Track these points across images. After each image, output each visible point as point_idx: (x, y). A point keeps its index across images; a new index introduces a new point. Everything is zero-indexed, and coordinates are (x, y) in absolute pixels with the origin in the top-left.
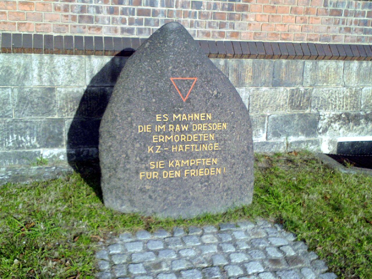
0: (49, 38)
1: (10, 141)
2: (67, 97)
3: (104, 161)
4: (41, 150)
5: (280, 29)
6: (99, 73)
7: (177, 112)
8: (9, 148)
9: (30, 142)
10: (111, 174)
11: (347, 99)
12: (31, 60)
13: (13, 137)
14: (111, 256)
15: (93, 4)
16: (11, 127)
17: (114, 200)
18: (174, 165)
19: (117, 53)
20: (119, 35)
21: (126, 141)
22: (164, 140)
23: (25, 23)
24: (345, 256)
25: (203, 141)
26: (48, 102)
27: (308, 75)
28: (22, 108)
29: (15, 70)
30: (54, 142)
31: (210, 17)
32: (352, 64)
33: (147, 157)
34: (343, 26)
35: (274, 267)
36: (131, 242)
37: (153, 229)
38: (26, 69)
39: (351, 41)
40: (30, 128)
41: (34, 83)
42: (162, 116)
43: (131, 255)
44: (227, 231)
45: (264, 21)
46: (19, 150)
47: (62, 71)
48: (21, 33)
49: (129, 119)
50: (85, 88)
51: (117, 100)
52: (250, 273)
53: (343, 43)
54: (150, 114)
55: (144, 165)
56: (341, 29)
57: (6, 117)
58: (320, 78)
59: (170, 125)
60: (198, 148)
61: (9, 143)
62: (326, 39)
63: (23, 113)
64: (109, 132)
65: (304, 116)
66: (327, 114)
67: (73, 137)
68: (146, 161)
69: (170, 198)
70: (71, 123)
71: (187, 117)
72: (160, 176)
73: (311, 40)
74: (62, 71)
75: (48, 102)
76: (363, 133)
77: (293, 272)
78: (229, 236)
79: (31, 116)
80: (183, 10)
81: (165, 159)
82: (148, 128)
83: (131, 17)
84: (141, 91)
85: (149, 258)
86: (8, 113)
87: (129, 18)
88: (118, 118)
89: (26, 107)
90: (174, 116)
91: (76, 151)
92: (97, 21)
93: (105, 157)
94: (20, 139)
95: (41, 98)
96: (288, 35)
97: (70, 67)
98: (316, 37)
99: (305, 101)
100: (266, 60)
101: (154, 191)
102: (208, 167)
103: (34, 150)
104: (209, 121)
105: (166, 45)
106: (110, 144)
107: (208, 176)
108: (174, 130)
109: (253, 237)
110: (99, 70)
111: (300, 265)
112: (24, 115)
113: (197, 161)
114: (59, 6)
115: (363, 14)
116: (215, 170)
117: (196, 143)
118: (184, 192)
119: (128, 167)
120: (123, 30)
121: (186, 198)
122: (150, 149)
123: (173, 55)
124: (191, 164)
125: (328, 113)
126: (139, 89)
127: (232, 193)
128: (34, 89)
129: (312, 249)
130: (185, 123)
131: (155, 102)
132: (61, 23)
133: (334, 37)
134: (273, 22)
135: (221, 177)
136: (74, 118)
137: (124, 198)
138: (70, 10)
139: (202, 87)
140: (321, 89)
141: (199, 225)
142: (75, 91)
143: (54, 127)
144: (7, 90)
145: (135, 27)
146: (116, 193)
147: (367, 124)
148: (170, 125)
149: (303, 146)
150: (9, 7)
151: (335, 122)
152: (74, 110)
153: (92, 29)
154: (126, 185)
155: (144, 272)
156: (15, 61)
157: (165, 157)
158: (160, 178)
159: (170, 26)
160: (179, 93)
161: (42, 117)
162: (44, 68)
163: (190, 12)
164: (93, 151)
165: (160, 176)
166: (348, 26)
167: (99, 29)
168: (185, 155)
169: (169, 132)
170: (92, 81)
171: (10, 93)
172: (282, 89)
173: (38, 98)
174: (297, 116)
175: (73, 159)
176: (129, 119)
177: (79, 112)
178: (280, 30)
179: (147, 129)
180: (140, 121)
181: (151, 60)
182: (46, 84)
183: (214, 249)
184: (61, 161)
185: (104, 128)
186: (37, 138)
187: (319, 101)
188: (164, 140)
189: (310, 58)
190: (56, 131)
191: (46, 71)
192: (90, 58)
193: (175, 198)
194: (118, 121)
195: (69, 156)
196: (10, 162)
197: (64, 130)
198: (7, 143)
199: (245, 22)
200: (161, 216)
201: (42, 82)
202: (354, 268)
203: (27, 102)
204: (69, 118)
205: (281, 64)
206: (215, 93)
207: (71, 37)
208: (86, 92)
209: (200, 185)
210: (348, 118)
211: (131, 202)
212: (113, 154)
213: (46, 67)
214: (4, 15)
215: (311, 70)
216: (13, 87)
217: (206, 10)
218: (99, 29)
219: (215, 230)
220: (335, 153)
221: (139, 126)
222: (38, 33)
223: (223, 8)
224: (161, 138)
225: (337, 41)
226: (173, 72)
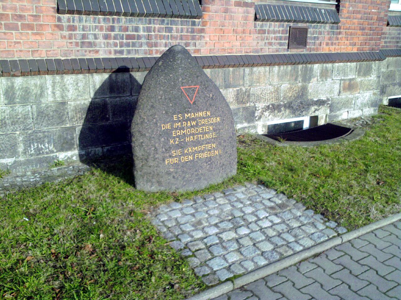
0: (58, 61)
1: (32, 149)
2: (76, 109)
3: (137, 154)
4: (57, 154)
5: (227, 46)
6: (100, 87)
7: (188, 112)
8: (31, 155)
9: (48, 148)
10: (144, 163)
11: (272, 94)
12: (46, 80)
13: (34, 145)
14: (163, 222)
15: (92, 32)
16: (32, 137)
17: (145, 183)
18: (188, 151)
19: (114, 70)
20: (113, 56)
21: (154, 137)
22: (181, 133)
23: (37, 51)
24: (313, 199)
25: (205, 132)
26: (61, 114)
27: (247, 78)
28: (40, 121)
29: (33, 90)
30: (67, 146)
31: (179, 39)
32: (274, 69)
33: (170, 147)
34: (267, 41)
35: (274, 212)
36: (170, 211)
37: (181, 200)
38: (42, 88)
39: (273, 52)
40: (48, 137)
41: (49, 99)
42: (178, 116)
43: (176, 219)
44: (230, 194)
45: (216, 40)
46: (40, 156)
47: (71, 88)
48: (35, 58)
49: (155, 120)
50: (90, 100)
51: (143, 107)
52: (261, 218)
53: (268, 54)
54: (169, 115)
55: (168, 154)
56: (265, 43)
57: (27, 129)
58: (255, 80)
59: (184, 122)
60: (203, 137)
61: (31, 151)
62: (257, 51)
63: (42, 125)
64: (140, 131)
65: (246, 109)
66: (260, 106)
67: (83, 141)
68: (170, 151)
69: (187, 176)
70: (80, 129)
71: (195, 115)
72: (180, 161)
73: (247, 52)
74: (71, 88)
75: (61, 114)
76: (283, 118)
77: (286, 213)
78: (233, 197)
79: (48, 126)
80: (159, 34)
81: (182, 148)
82: (168, 126)
83: (121, 41)
84: (161, 98)
85: (191, 219)
86: (29, 126)
87: (120, 42)
88: (146, 121)
89: (44, 119)
90: (186, 115)
91: (85, 152)
92: (95, 46)
93: (138, 151)
94: (40, 147)
95: (56, 111)
96: (232, 49)
97: (77, 84)
98: (250, 50)
99: (246, 97)
100: (220, 69)
101: (176, 173)
102: (210, 150)
103: (52, 155)
104: (209, 117)
105: (175, 63)
106: (141, 140)
107: (210, 157)
108: (187, 125)
109: (249, 195)
110: (100, 85)
111: (288, 208)
112: (42, 126)
113: (203, 147)
114: (64, 34)
115: (279, 32)
116: (214, 152)
117: (201, 133)
118: (196, 171)
119: (157, 156)
120: (116, 52)
121: (197, 175)
122: (172, 142)
123: (182, 70)
124: (199, 149)
125: (261, 105)
126: (160, 97)
127: (225, 168)
128: (49, 104)
129: (290, 197)
130: (194, 119)
131: (172, 106)
132: (66, 49)
133: (261, 49)
134: (222, 40)
135: (218, 157)
136: (83, 125)
137: (154, 180)
138: (73, 38)
139: (202, 92)
140: (256, 88)
141: (209, 193)
142: (82, 103)
143: (67, 134)
144: (27, 107)
145: (124, 48)
146: (147, 178)
147: (285, 110)
148: (184, 122)
149: (247, 131)
150: (23, 38)
151: (265, 111)
152: (82, 118)
153: (92, 52)
154: (155, 171)
155: (193, 228)
156: (33, 82)
157: (181, 146)
158: (180, 162)
159: (176, 49)
160: (188, 98)
161: (57, 127)
162: (57, 87)
163: (165, 35)
164: (98, 150)
165: (180, 161)
166: (270, 41)
167: (97, 52)
168: (195, 144)
169: (183, 128)
170: (96, 94)
171: (30, 109)
172: (231, 90)
173: (53, 111)
174: (241, 109)
175: (84, 159)
176: (155, 120)
177: (87, 120)
178: (227, 46)
179: (168, 126)
180: (163, 121)
181: (165, 74)
182: (59, 99)
183: (229, 208)
184: (74, 162)
185: (135, 129)
186: (54, 144)
187: (255, 97)
188: (181, 133)
189: (248, 66)
190: (69, 137)
191: (58, 89)
192: (92, 75)
193: (190, 176)
194: (146, 123)
195: (81, 156)
196: (33, 167)
197: (75, 136)
198: (29, 151)
199: (203, 41)
200: (181, 191)
201: (55, 98)
202: (322, 204)
203: (44, 115)
204: (79, 125)
205: (229, 71)
206: (211, 95)
207: (76, 59)
208: (91, 103)
209: (205, 164)
210: (274, 107)
211: (159, 183)
212: (144, 148)
213: (58, 86)
214: (19, 44)
215: (248, 75)
216: (31, 104)
217: (175, 34)
218: (97, 52)
219: (222, 195)
220: (266, 133)
221: (162, 125)
222: (49, 58)
223: (187, 32)
224: (178, 132)
225: (264, 53)
226: (183, 83)
